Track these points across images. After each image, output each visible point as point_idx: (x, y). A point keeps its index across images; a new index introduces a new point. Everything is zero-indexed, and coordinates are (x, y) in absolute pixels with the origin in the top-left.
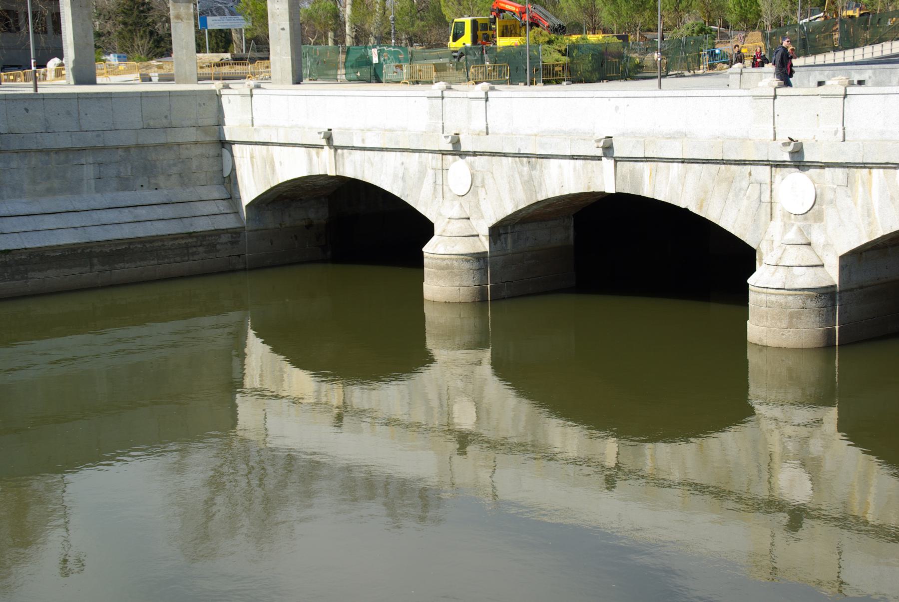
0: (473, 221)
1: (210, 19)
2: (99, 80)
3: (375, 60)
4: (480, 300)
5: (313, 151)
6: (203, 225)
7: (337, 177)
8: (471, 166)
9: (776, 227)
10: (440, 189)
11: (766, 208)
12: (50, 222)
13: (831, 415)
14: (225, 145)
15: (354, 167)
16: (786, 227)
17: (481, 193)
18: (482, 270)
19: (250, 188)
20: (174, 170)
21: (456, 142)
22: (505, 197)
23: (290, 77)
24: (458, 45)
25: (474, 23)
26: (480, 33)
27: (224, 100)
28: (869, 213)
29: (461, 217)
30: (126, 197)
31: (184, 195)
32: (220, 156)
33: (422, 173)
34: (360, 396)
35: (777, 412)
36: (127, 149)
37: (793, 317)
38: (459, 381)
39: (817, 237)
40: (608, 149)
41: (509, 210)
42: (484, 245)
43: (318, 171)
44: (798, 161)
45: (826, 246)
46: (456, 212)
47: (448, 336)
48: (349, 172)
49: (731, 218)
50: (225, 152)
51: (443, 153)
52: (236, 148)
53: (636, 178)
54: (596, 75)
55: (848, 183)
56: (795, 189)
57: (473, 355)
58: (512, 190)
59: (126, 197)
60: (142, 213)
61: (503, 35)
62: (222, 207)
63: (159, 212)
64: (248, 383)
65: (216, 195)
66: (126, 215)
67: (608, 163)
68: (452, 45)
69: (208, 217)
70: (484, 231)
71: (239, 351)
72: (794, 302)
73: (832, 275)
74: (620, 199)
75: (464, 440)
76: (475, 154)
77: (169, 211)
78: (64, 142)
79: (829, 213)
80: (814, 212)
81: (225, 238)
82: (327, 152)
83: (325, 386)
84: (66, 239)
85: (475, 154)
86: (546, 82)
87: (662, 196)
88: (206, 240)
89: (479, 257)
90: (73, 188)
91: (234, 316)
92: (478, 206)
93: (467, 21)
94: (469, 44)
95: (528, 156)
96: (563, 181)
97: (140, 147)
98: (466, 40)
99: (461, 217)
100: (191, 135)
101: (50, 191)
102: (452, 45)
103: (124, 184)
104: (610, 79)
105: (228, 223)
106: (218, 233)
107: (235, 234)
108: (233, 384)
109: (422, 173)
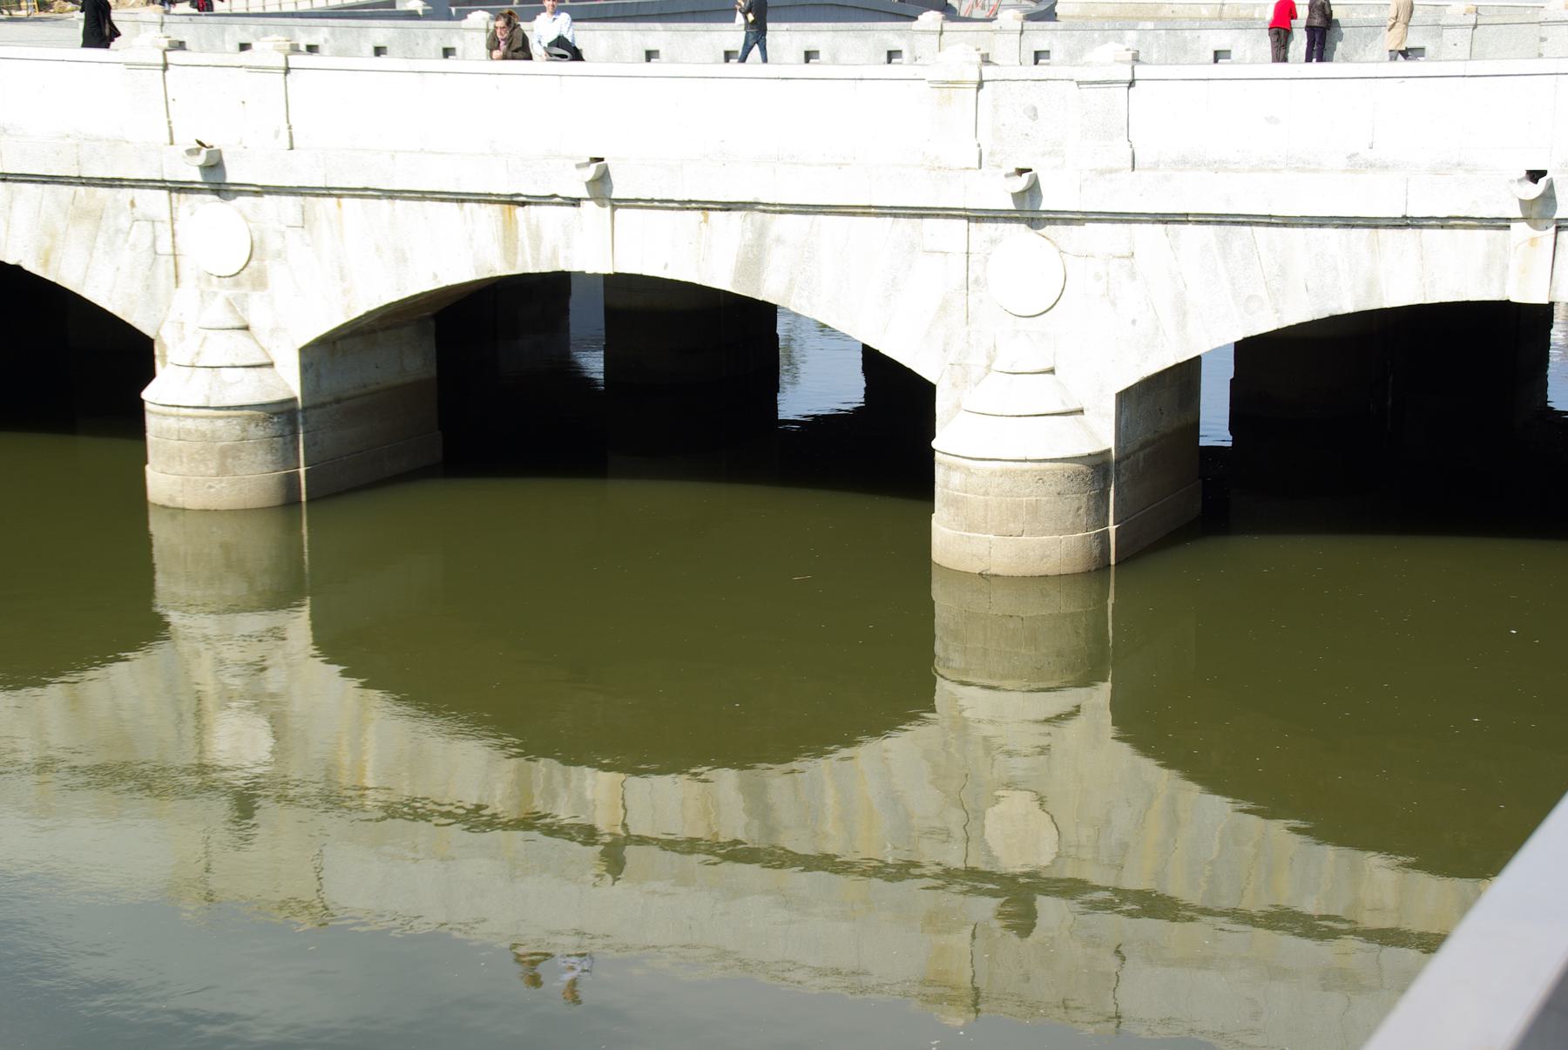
11: (165, 265)
13: (299, 624)
21: (214, 167)
37: (227, 457)
39: (258, 312)
72: (227, 430)
73: (288, 382)
79: (276, 273)
80: (250, 272)
89: (1098, 466)
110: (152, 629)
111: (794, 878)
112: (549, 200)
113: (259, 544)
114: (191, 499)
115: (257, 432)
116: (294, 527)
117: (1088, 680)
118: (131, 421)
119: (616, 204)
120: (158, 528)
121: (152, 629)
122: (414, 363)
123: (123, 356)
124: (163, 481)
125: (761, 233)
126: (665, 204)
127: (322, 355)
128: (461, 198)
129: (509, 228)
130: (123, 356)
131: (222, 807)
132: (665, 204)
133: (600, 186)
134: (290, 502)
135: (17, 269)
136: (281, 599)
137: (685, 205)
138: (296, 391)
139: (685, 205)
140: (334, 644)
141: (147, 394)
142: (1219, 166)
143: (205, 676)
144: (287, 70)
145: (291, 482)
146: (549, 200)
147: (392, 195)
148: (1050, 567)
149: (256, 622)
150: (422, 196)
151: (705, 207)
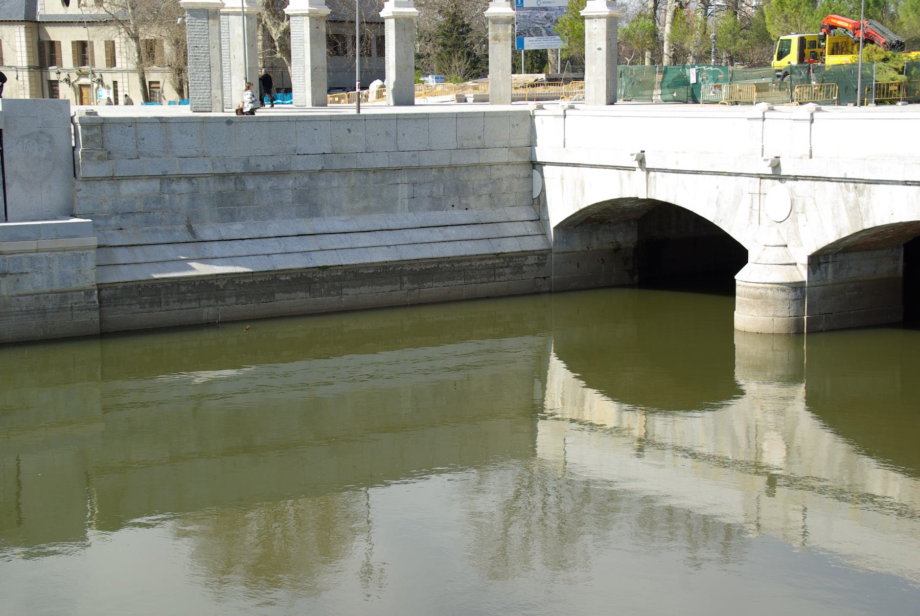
3: (693, 80)
4: (796, 331)
6: (510, 246)
11: (756, 214)
13: (800, 391)
17: (801, 217)
18: (799, 300)
19: (560, 208)
20: (485, 191)
21: (776, 166)
22: (830, 221)
24: (783, 63)
25: (802, 41)
26: (807, 51)
27: (537, 120)
30: (438, 217)
31: (493, 215)
32: (530, 177)
36: (441, 169)
47: (759, 369)
50: (536, 173)
51: (762, 177)
59: (438, 217)
61: (833, 52)
62: (530, 228)
63: (468, 232)
65: (525, 216)
66: (437, 235)
68: (776, 64)
69: (516, 238)
71: (540, 374)
73: (802, 274)
76: (796, 178)
78: (382, 161)
81: (531, 260)
82: (640, 174)
84: (379, 257)
85: (796, 178)
89: (797, 287)
90: (388, 207)
91: (536, 340)
93: (794, 39)
94: (795, 62)
95: (855, 181)
98: (792, 58)
100: (503, 156)
101: (366, 210)
103: (437, 204)
105: (535, 244)
106: (524, 254)
107: (542, 255)
108: (535, 410)
110: (736, 392)
113: (781, 354)
114: (751, 328)
116: (799, 345)
118: (729, 290)
120: (738, 341)
121: (736, 392)
122: (891, 266)
127: (816, 261)
130: (737, 256)
131: (761, 482)
134: (799, 332)
136: (793, 379)
138: (806, 279)
140: (814, 403)
141: (737, 277)
144: (764, 119)
145: (798, 324)
150: (567, 165)
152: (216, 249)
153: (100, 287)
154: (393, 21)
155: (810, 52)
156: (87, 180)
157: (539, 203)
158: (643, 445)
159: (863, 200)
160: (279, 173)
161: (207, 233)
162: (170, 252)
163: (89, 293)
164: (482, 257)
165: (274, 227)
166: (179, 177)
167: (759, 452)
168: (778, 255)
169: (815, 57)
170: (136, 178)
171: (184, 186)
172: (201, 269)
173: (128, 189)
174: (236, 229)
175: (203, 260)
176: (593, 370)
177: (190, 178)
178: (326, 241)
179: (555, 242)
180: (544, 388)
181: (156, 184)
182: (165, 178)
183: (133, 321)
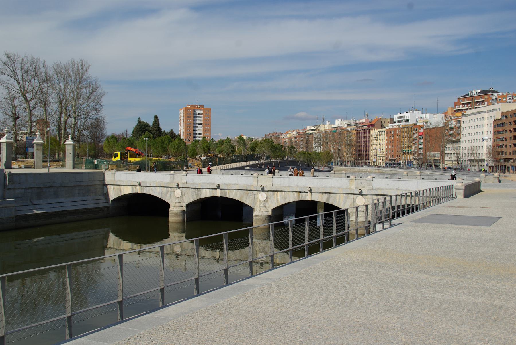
0: (182, 203)
1: (29, 149)
2: (13, 166)
3: (96, 163)
4: (184, 221)
5: (134, 187)
6: (101, 205)
7: (141, 193)
8: (181, 191)
9: (258, 203)
10: (172, 195)
11: (256, 199)
12: (70, 204)
13: (185, 234)
14: (106, 185)
15: (146, 191)
16: (260, 204)
17: (184, 197)
18: (184, 215)
19: (113, 195)
21: (178, 185)
22: (191, 197)
23: (72, 167)
24: (116, 159)
25: (121, 153)
26: (122, 156)
27: (106, 174)
28: (278, 201)
29: (178, 203)
30: (84, 198)
32: (103, 188)
33: (167, 192)
34: (145, 247)
35: (260, 242)
36: (85, 186)
37: (264, 222)
38: (177, 241)
39: (267, 205)
40: (219, 187)
41: (192, 200)
42: (185, 209)
43: (135, 192)
44: (263, 190)
45: (269, 207)
46: (177, 201)
47: (176, 230)
48: (145, 192)
49: (247, 201)
50: (105, 187)
51: (174, 187)
52: (109, 186)
53: (225, 193)
54: (163, 170)
55: (273, 195)
56: (262, 196)
57: (181, 235)
58: (193, 196)
59: (84, 198)
60: (88, 202)
61: (130, 157)
62: (104, 201)
64: (108, 246)
65: (103, 198)
66: (85, 203)
67: (218, 190)
68: (114, 159)
69: (102, 204)
70: (184, 205)
71: (106, 238)
72: (264, 218)
73: (270, 213)
74: (221, 198)
75: (177, 256)
76: (183, 188)
77: (92, 202)
78: (73, 184)
79: (270, 201)
80: (266, 201)
81: (106, 209)
82: (138, 187)
83: (135, 245)
84: (74, 208)
85: (183, 188)
86: (151, 171)
87: (231, 197)
88: (101, 209)
89: (184, 211)
91: (106, 229)
92: (183, 200)
93: (119, 153)
94: (119, 159)
95: (197, 188)
96: (206, 194)
97: (87, 185)
98: (118, 158)
99: (178, 203)
100: (98, 183)
102: (114, 159)
104: (167, 171)
105: (106, 205)
106: (105, 207)
107: (108, 207)
108: (105, 247)
109: (167, 192)
111: (204, 260)
112: (304, 192)
115: (181, 213)
117: (184, 233)
119: (312, 193)
123: (168, 206)
124: (171, 219)
125: (329, 196)
126: (318, 193)
127: (187, 206)
128: (293, 192)
129: (299, 195)
131: (174, 257)
132: (318, 193)
133: (140, 184)
135: (237, 200)
136: (183, 232)
137: (320, 193)
139: (320, 193)
142: (382, 189)
143: (257, 249)
146: (304, 192)
147: (284, 191)
148: (174, 221)
149: (265, 241)
151: (323, 193)
152: (38, 207)
153: (16, 216)
154: (5, 144)
155: (124, 157)
156: (9, 189)
157: (106, 195)
158: (139, 252)
159: (199, 192)
160: (51, 187)
161: (35, 202)
162: (28, 207)
163: (13, 218)
164: (96, 208)
165: (49, 201)
166: (29, 188)
167: (173, 250)
168: (178, 205)
169: (125, 158)
170: (19, 188)
171: (29, 191)
172: (37, 212)
173: (17, 191)
174: (41, 201)
175: (36, 209)
176: (122, 235)
177: (31, 188)
178: (62, 204)
179: (111, 204)
180: (107, 241)
181: (23, 190)
182: (26, 189)
183: (24, 226)
